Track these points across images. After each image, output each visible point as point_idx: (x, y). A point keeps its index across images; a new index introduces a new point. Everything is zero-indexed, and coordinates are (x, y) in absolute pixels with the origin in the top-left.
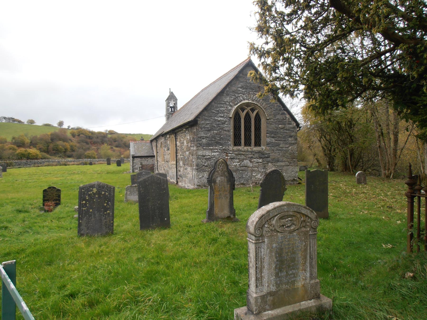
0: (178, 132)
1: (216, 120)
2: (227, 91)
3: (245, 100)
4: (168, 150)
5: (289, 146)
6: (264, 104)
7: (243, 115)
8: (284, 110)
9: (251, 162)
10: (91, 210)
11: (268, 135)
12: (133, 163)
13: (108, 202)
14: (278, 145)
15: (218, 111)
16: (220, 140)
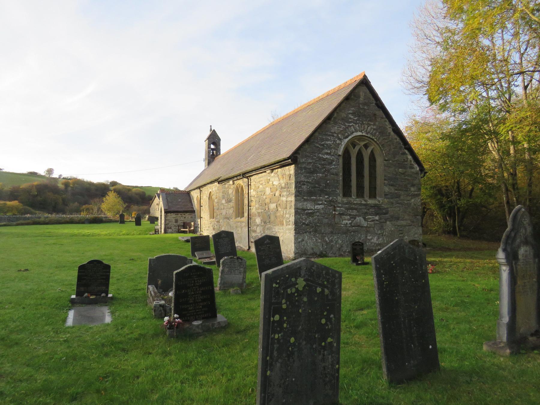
2: (335, 118)
3: (357, 132)
5: (412, 199)
6: (381, 138)
7: (354, 153)
8: (406, 148)
9: (365, 219)
10: (292, 340)
13: (329, 315)
14: (398, 196)
15: (323, 145)
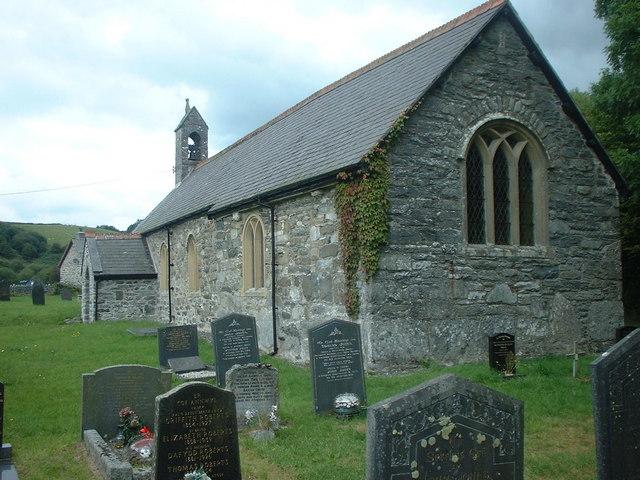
0: (279, 203)
1: (422, 165)
3: (494, 111)
4: (233, 254)
5: (603, 246)
7: (489, 152)
9: (512, 288)
11: (552, 212)
12: (97, 294)
15: (426, 139)
16: (433, 224)
